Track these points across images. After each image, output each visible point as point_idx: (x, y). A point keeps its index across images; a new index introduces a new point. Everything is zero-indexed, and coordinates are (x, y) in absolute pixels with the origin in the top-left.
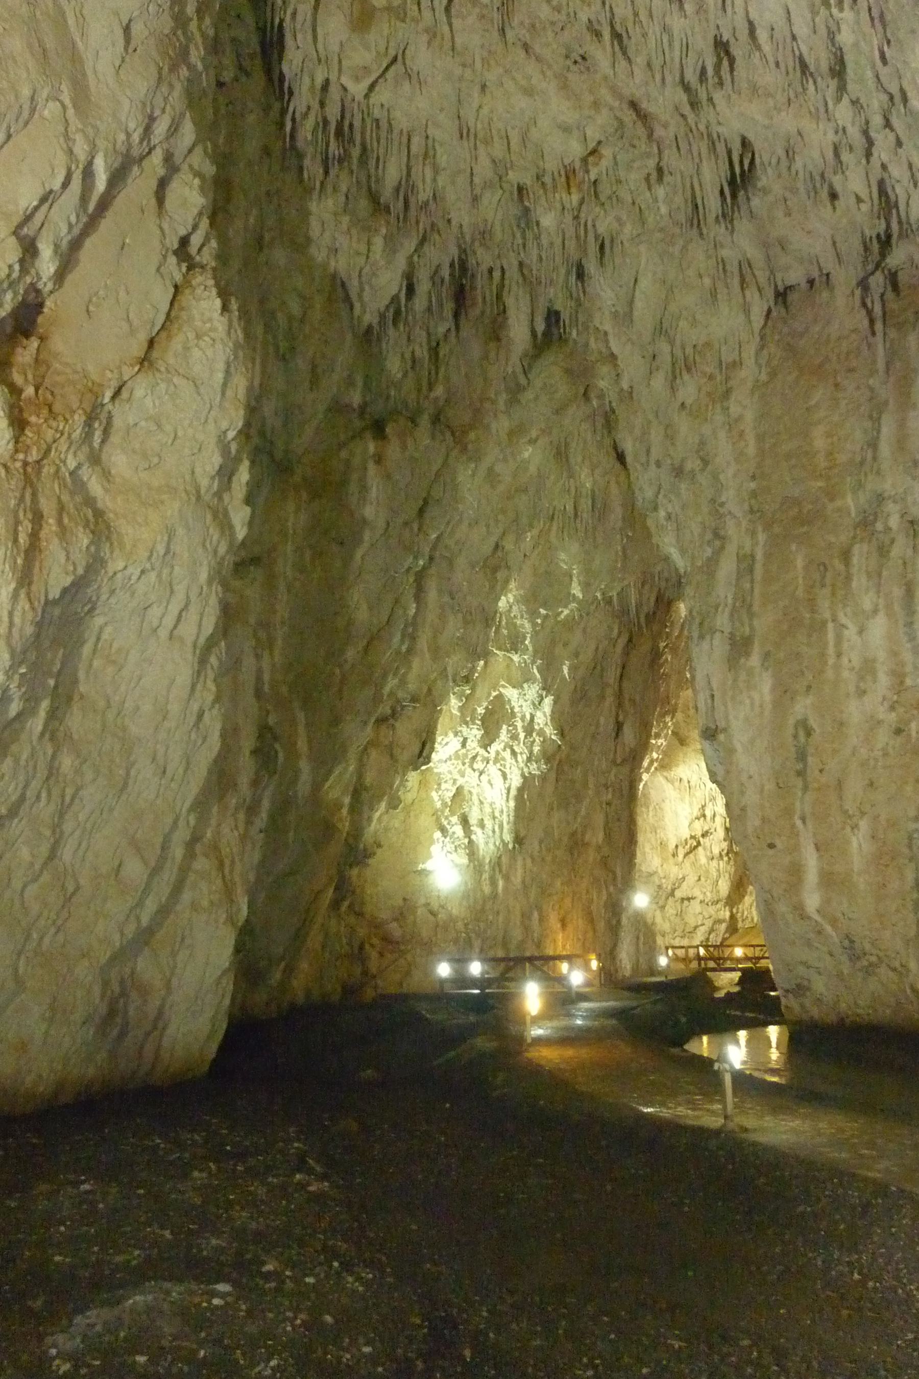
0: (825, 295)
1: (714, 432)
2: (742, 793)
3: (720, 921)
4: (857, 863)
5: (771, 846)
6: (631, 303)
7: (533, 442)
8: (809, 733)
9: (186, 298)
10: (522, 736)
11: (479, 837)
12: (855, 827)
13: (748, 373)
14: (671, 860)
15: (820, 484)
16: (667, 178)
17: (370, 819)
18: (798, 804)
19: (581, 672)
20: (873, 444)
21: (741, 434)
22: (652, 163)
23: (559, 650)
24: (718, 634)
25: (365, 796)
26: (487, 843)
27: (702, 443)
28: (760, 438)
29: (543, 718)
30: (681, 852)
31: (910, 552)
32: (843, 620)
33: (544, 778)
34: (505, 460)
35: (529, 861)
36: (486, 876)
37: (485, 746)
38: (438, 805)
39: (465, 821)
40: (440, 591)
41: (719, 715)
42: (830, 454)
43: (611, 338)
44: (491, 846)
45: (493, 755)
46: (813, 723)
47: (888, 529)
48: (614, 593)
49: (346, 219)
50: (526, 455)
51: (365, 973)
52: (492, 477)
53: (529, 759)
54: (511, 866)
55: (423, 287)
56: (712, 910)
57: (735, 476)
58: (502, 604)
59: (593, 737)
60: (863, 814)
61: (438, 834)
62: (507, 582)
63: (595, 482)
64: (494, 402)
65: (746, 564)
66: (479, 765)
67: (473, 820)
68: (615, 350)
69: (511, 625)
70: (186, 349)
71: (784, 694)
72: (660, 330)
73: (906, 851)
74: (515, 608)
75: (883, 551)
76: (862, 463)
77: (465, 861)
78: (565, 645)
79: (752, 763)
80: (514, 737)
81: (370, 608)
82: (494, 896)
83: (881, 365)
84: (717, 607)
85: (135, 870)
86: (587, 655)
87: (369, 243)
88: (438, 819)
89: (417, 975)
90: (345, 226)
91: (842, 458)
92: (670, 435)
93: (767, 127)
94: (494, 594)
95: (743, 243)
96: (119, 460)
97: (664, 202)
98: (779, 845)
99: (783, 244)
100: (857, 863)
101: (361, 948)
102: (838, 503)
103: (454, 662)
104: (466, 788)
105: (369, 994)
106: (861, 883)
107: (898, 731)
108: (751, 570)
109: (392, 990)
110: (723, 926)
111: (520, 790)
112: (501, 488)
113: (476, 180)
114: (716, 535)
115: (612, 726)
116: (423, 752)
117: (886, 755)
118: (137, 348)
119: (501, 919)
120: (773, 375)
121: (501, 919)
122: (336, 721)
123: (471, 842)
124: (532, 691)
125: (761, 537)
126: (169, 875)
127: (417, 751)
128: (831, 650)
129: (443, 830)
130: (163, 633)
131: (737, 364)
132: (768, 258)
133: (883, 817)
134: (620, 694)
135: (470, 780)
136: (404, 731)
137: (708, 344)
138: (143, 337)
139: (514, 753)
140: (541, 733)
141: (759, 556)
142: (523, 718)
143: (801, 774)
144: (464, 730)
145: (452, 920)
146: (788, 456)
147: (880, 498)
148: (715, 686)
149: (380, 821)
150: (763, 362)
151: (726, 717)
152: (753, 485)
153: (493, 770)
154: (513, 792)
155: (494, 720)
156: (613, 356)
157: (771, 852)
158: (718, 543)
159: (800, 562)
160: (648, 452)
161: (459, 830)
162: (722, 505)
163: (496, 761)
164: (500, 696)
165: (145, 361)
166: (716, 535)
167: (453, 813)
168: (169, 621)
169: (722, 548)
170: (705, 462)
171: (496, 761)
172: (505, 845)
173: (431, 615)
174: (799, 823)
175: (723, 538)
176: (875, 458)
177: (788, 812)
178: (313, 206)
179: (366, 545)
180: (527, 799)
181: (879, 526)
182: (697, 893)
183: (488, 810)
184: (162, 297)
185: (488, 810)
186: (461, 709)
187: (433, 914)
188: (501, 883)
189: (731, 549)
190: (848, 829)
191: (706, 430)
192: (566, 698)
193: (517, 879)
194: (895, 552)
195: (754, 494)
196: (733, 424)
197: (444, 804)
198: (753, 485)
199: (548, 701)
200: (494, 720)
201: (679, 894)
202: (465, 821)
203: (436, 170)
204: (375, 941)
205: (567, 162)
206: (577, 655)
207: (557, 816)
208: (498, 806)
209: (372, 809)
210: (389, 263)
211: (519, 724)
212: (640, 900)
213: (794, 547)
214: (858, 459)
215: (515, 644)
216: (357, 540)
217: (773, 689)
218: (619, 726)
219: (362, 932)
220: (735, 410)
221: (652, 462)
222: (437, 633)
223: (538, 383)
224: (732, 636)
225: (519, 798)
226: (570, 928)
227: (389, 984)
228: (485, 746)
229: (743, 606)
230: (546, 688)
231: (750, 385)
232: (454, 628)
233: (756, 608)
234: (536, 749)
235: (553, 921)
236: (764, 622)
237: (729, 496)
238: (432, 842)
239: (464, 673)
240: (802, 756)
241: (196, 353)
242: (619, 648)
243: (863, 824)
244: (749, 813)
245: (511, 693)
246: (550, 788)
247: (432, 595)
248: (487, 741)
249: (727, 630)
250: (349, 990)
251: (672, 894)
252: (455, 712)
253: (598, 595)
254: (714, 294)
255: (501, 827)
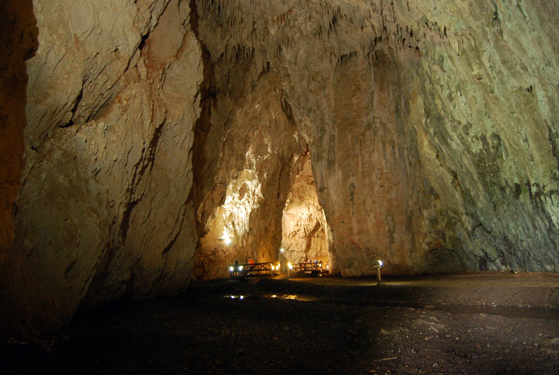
0: (355, 58)
1: (321, 98)
2: (333, 207)
3: (302, 258)
4: (370, 225)
5: (343, 222)
6: (296, 58)
7: (259, 103)
8: (354, 187)
9: (187, 39)
10: (251, 196)
11: (237, 228)
12: (369, 215)
13: (332, 81)
14: (288, 239)
15: (355, 113)
16: (311, 20)
17: (206, 222)
18: (351, 209)
19: (270, 176)
20: (371, 102)
21: (330, 99)
22: (308, 14)
23: (263, 169)
24: (324, 160)
25: (205, 215)
26: (241, 231)
27: (317, 102)
28: (336, 100)
29: (258, 191)
30: (291, 236)
31: (384, 133)
32: (364, 154)
33: (258, 209)
34: (250, 108)
35: (253, 236)
36: (240, 240)
37: (240, 199)
38: (225, 218)
39: (233, 224)
40: (229, 150)
41: (325, 184)
42: (357, 105)
43: (288, 69)
44: (242, 231)
45: (242, 203)
46: (355, 184)
47: (376, 127)
48: (280, 152)
49: (209, 28)
50: (257, 107)
51: (204, 271)
52: (246, 114)
53: (254, 204)
54: (248, 237)
55: (230, 51)
56: (300, 254)
57: (328, 111)
58: (247, 154)
59: (272, 197)
60: (372, 211)
61: (225, 228)
62: (249, 147)
63: (276, 117)
64: (247, 90)
65: (332, 138)
66: (238, 206)
67: (236, 223)
68: (290, 73)
69: (249, 161)
70: (188, 55)
71: (346, 177)
72: (306, 68)
73: (386, 221)
74: (251, 155)
75: (375, 133)
76: (368, 107)
77: (233, 236)
78: (265, 168)
79: (335, 197)
80: (249, 197)
81: (211, 153)
82: (243, 247)
83: (373, 78)
84: (323, 151)
85: (171, 221)
86: (271, 171)
87: (216, 36)
88: (225, 223)
89: (221, 272)
90: (209, 30)
91: (362, 106)
92: (307, 100)
93: (348, 4)
94: (246, 151)
95: (333, 42)
96: (167, 88)
97: (309, 28)
98: (345, 222)
99: (344, 41)
100: (370, 225)
101: (203, 263)
102: (361, 119)
103: (233, 172)
104: (234, 213)
105: (206, 278)
106: (372, 231)
107: (381, 186)
108: (334, 139)
109: (213, 277)
110: (304, 259)
111: (251, 213)
112: (249, 117)
113: (255, 16)
114: (322, 129)
115: (277, 194)
116: (222, 202)
117: (378, 193)
118: (174, 52)
119: (245, 254)
120: (338, 82)
121: (245, 254)
122: (202, 188)
123: (235, 230)
124: (255, 182)
125: (337, 130)
126: (178, 225)
127: (220, 200)
128: (360, 163)
129: (227, 226)
130: (179, 145)
131: (328, 78)
132: (339, 47)
133: (378, 212)
134: (279, 184)
135: (235, 210)
136: (216, 194)
137: (319, 72)
138: (176, 49)
139: (249, 202)
140: (257, 195)
141: (336, 134)
142: (252, 191)
143: (352, 200)
144: (234, 194)
145: (230, 254)
146: (345, 105)
147: (374, 118)
148: (323, 175)
149: (210, 223)
150: (335, 78)
151: (328, 185)
152: (334, 114)
153: (242, 207)
154: (249, 214)
155: (243, 191)
156: (288, 76)
157: (343, 224)
158: (323, 132)
159: (349, 137)
160: (299, 105)
161: (231, 226)
162: (324, 120)
163: (243, 204)
164: (245, 184)
165: (177, 57)
166: (322, 129)
167: (229, 221)
168: (181, 141)
169: (324, 133)
170: (319, 108)
171: (243, 204)
172: (246, 231)
173: (226, 157)
174: (351, 215)
175: (324, 130)
176: (372, 106)
177: (348, 212)
178: (199, 23)
179: (211, 132)
180: (253, 216)
181: (374, 126)
182: (296, 249)
183: (240, 220)
184: (180, 37)
185: (240, 220)
186: (233, 188)
187: (225, 253)
188: (245, 243)
189: (327, 133)
190: (367, 216)
191: (318, 98)
192: (265, 184)
193: (250, 241)
194: (379, 133)
195: (334, 117)
196: (327, 96)
197: (227, 218)
198: (334, 114)
199: (260, 185)
200: (243, 191)
201: (290, 249)
202: (233, 224)
203: (242, 13)
204: (207, 262)
205: (283, 12)
206: (268, 171)
207: (262, 221)
208: (244, 219)
209: (207, 218)
210: (221, 42)
211: (250, 193)
212: (282, 250)
213: (347, 132)
214: (367, 106)
215: (251, 167)
216: (208, 131)
217: (342, 175)
218: (279, 195)
219: (202, 259)
220: (327, 92)
221: (301, 107)
222: (227, 163)
223: (261, 85)
224: (328, 160)
225: (250, 216)
226: (265, 257)
227: (212, 275)
228: (240, 199)
229: (331, 150)
230: (259, 181)
231: (332, 84)
232: (233, 161)
233: (335, 151)
234: (256, 200)
235: (261, 255)
236: (338, 155)
237: (326, 117)
238: (223, 230)
239: (235, 176)
240: (352, 194)
241: (191, 56)
242: (279, 170)
243: (372, 215)
244: (336, 212)
245: (248, 183)
246: (259, 213)
247: (227, 150)
248: (241, 197)
249: (327, 157)
250: (199, 278)
251: (288, 250)
252: (231, 189)
253: (276, 152)
254: (322, 56)
255: (245, 225)
